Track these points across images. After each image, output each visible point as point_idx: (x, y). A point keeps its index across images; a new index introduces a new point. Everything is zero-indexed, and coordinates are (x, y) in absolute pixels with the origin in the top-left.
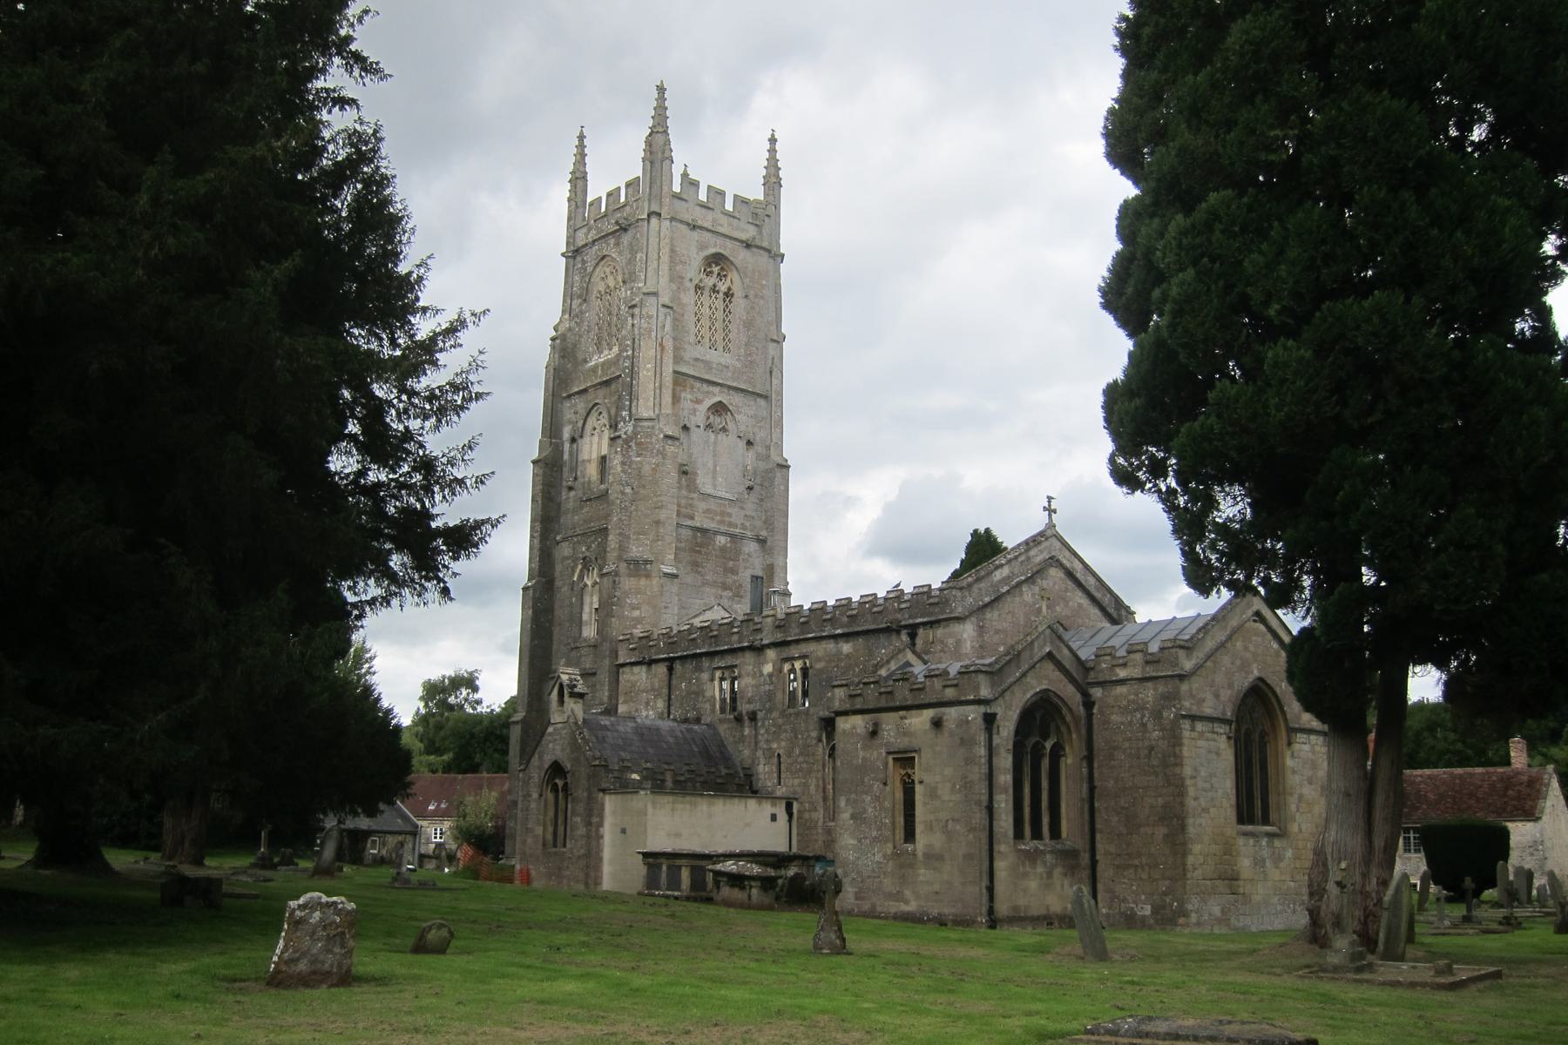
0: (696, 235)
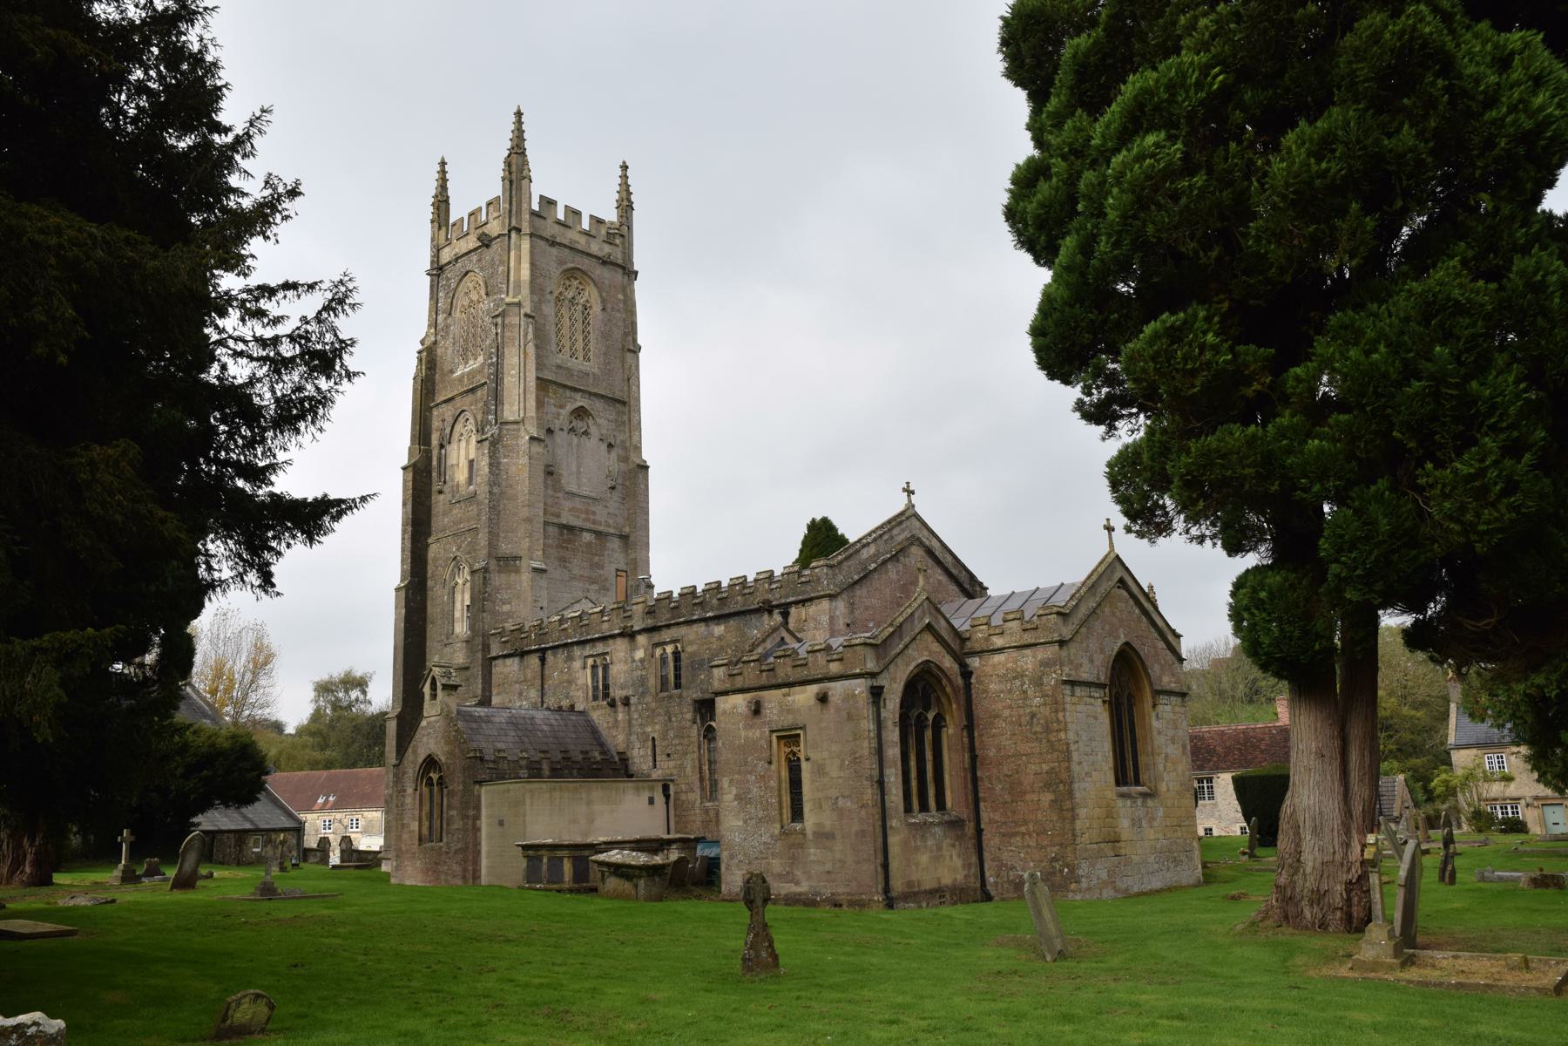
0: (554, 251)
